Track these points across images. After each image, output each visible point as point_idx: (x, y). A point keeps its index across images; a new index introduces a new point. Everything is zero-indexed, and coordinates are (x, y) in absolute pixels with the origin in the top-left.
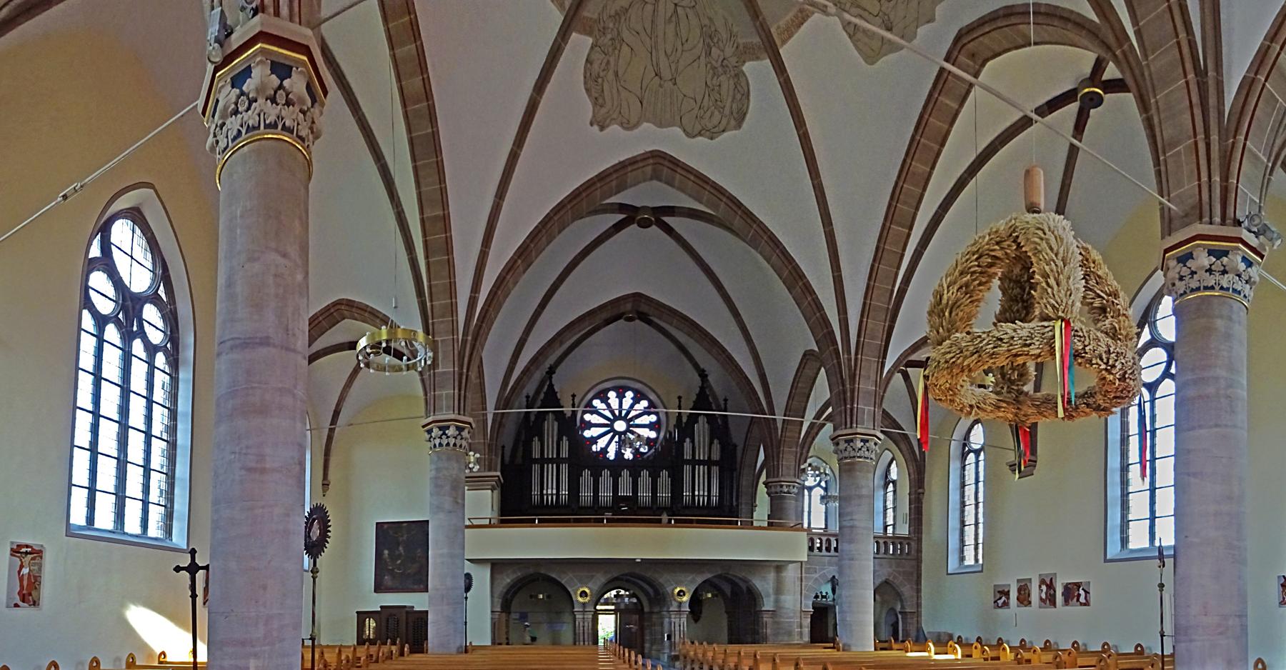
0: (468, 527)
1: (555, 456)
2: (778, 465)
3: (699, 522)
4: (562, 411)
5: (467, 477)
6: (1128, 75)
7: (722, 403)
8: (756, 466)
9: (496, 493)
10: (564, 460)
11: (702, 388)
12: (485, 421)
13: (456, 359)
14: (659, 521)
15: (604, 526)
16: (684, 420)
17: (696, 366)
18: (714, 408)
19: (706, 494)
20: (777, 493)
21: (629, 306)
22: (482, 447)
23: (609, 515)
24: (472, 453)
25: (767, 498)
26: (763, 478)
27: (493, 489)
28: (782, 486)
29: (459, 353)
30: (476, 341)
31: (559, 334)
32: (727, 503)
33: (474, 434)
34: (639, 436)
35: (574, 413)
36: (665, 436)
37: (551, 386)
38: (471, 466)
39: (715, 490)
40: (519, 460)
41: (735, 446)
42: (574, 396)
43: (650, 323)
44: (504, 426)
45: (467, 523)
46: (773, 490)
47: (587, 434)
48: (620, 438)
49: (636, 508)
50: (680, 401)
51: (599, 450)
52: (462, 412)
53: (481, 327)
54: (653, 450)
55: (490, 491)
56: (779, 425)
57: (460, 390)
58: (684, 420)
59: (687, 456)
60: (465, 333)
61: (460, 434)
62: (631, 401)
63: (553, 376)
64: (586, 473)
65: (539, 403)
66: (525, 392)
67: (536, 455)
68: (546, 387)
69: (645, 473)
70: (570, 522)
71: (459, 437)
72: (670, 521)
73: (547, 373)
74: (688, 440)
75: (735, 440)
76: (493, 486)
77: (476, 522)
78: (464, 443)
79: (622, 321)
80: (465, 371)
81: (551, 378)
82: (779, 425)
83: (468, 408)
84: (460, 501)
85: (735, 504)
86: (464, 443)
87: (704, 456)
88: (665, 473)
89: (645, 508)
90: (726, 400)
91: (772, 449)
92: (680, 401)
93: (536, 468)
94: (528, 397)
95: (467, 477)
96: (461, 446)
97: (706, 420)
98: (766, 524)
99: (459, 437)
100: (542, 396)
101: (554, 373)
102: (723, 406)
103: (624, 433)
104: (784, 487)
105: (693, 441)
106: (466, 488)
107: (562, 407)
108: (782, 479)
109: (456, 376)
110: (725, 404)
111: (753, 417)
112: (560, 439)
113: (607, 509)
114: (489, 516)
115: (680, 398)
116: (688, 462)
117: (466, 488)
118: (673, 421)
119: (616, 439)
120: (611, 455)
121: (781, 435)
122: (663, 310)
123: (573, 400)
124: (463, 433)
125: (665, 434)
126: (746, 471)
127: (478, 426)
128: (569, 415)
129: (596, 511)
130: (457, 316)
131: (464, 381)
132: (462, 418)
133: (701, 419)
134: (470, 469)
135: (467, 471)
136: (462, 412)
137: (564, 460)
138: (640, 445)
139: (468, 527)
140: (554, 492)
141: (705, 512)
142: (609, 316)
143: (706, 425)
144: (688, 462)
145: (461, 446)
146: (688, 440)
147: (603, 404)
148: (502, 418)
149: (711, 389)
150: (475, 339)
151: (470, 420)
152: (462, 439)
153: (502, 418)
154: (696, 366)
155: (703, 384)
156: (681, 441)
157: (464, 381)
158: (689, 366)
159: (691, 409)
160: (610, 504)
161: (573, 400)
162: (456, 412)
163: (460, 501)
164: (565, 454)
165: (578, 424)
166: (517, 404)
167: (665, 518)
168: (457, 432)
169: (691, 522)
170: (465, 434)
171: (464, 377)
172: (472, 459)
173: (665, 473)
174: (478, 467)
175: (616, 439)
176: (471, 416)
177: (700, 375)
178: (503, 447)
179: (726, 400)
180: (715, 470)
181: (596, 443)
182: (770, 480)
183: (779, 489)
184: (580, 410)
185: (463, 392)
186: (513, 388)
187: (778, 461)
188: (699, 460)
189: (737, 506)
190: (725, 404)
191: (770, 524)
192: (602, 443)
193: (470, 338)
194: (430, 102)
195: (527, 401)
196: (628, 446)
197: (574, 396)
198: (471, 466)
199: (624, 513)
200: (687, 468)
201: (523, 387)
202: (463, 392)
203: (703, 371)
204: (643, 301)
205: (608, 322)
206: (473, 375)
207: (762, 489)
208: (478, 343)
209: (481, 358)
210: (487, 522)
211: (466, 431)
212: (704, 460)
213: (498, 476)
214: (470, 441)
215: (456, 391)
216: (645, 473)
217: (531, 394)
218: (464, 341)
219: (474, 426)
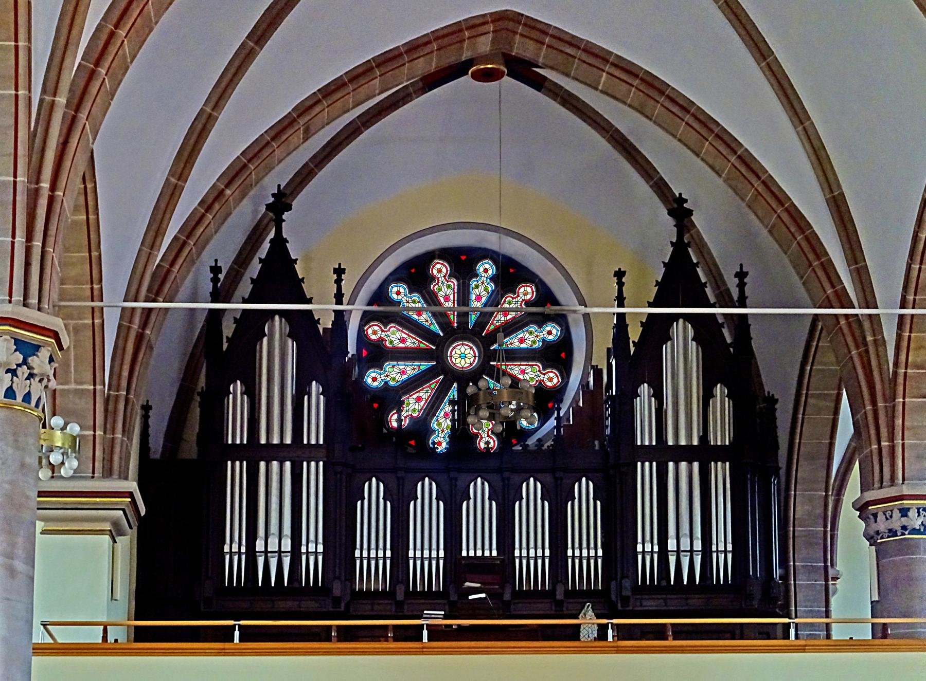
0: (40, 650)
1: (288, 441)
2: (892, 449)
3: (681, 633)
4: (310, 312)
5: (41, 494)
6: (833, 643)
7: (732, 284)
8: (830, 458)
9: (127, 543)
10: (312, 452)
11: (679, 248)
12: (98, 332)
13: (21, 151)
14: (573, 633)
15: (422, 651)
16: (634, 334)
17: (661, 188)
18: (712, 299)
19: (698, 546)
20: (893, 533)
21: (484, 44)
22: (85, 404)
23: (435, 617)
24: (57, 421)
25: (868, 552)
26: (853, 491)
27: (116, 532)
28: (904, 512)
29: (32, 136)
30: (78, 109)
31: (304, 109)
32: (754, 569)
33: (66, 364)
34: (515, 382)
35: (340, 318)
36: (584, 385)
37: (279, 243)
38: (55, 458)
39: (723, 539)
40: (190, 449)
41: (772, 401)
42: (339, 271)
43: (539, 83)
44: (150, 348)
45: (40, 637)
46: (882, 525)
47: (373, 379)
48: (461, 390)
49: (507, 596)
50: (621, 284)
51: (406, 423)
52: (34, 301)
53: (92, 74)
54: (552, 422)
55: (107, 538)
56: (889, 333)
57: (29, 237)
58: (634, 334)
59: (645, 436)
60: (51, 87)
61: (25, 362)
62: (491, 287)
63: (285, 216)
64: (374, 488)
65: (245, 287)
66: (207, 259)
67: (237, 434)
68: (266, 245)
69: (532, 488)
70: (328, 639)
71: (23, 371)
72: (603, 630)
73: (269, 207)
74: (644, 389)
75: (769, 387)
76: (116, 524)
77: (63, 636)
78: (37, 390)
79: (466, 80)
80: (45, 185)
81: (279, 223)
82: (889, 333)
83: (53, 290)
84: (19, 565)
85: (777, 572)
86: (37, 390)
87: (689, 436)
88: (584, 488)
89: (534, 595)
90: (741, 275)
91: (874, 402)
92: (621, 284)
93: (235, 471)
94: (216, 270)
95: (41, 494)
96: (27, 398)
97: (691, 333)
98: (866, 634)
99: (23, 371)
100: (255, 268)
101: (289, 208)
102: (735, 295)
103: (473, 376)
104: (913, 513)
105: (658, 394)
106: (40, 525)
107: (309, 301)
108: (906, 491)
109: (21, 199)
110: (741, 286)
111: (816, 316)
112: (301, 391)
113: (430, 598)
114: (104, 619)
115: (620, 274)
116: (647, 453)
117: (40, 525)
118: (605, 339)
119: (453, 393)
120: (441, 440)
121: (896, 364)
122: (569, 50)
123: (338, 281)
124: (33, 361)
125: (585, 375)
126: (803, 470)
127: (77, 344)
128: (327, 322)
129: (400, 605)
130: (29, 40)
131: (41, 212)
132: (31, 315)
133: (679, 330)
134: (52, 467)
135: (44, 474)
136: (34, 301)
137: (312, 452)
138: (519, 410)
139: (40, 650)
140: (287, 545)
141: (695, 601)
142: (433, 67)
143: (693, 346)
144: (647, 453)
145: (27, 398)
146: (644, 389)
147: (416, 296)
148: (144, 325)
149: (702, 248)
150: (76, 104)
151: (56, 323)
152: (31, 376)
153: (144, 325)
154: (661, 188)
155: (680, 235)
156: (627, 396)
157: (41, 212)
158: (643, 188)
159: (651, 305)
160: (438, 585)
161: (338, 281)
162: (18, 297)
163: (19, 565)
164: (315, 434)
165: (352, 348)
166: (186, 288)
167: (588, 622)
168: (20, 357)
169: (659, 633)
170: (39, 362)
171: (43, 202)
172: (58, 439)
173: (584, 488)
174: (75, 464)
175: (453, 393)
176: (58, 311)
177: (670, 213)
178: (146, 408)
179: (741, 275)
180: (721, 471)
181: (399, 406)
182: (871, 495)
183: (897, 522)
184: (355, 312)
185: (37, 243)
186: (179, 245)
187: (892, 438)
188: (677, 447)
189: (785, 577)
190: (741, 286)
191: (881, 632)
192: (413, 406)
193: (61, 100)
194: (48, 98)
195: (215, 280)
196: (484, 413)
197: (339, 271)
198: (55, 458)
199: (477, 610)
200: (645, 472)
201: (201, 247)
202: (37, 243)
203: (681, 200)
204: (520, 29)
205: (431, 82)
206: (69, 198)
207: (848, 516)
208: (83, 116)
209: (92, 153)
210: (94, 636)
211: (44, 354)
212: (689, 447)
213: (131, 495)
214: (53, 384)
215: (20, 239)
216: (532, 488)
217: (225, 265)
218: (47, 109)
219: (66, 343)
